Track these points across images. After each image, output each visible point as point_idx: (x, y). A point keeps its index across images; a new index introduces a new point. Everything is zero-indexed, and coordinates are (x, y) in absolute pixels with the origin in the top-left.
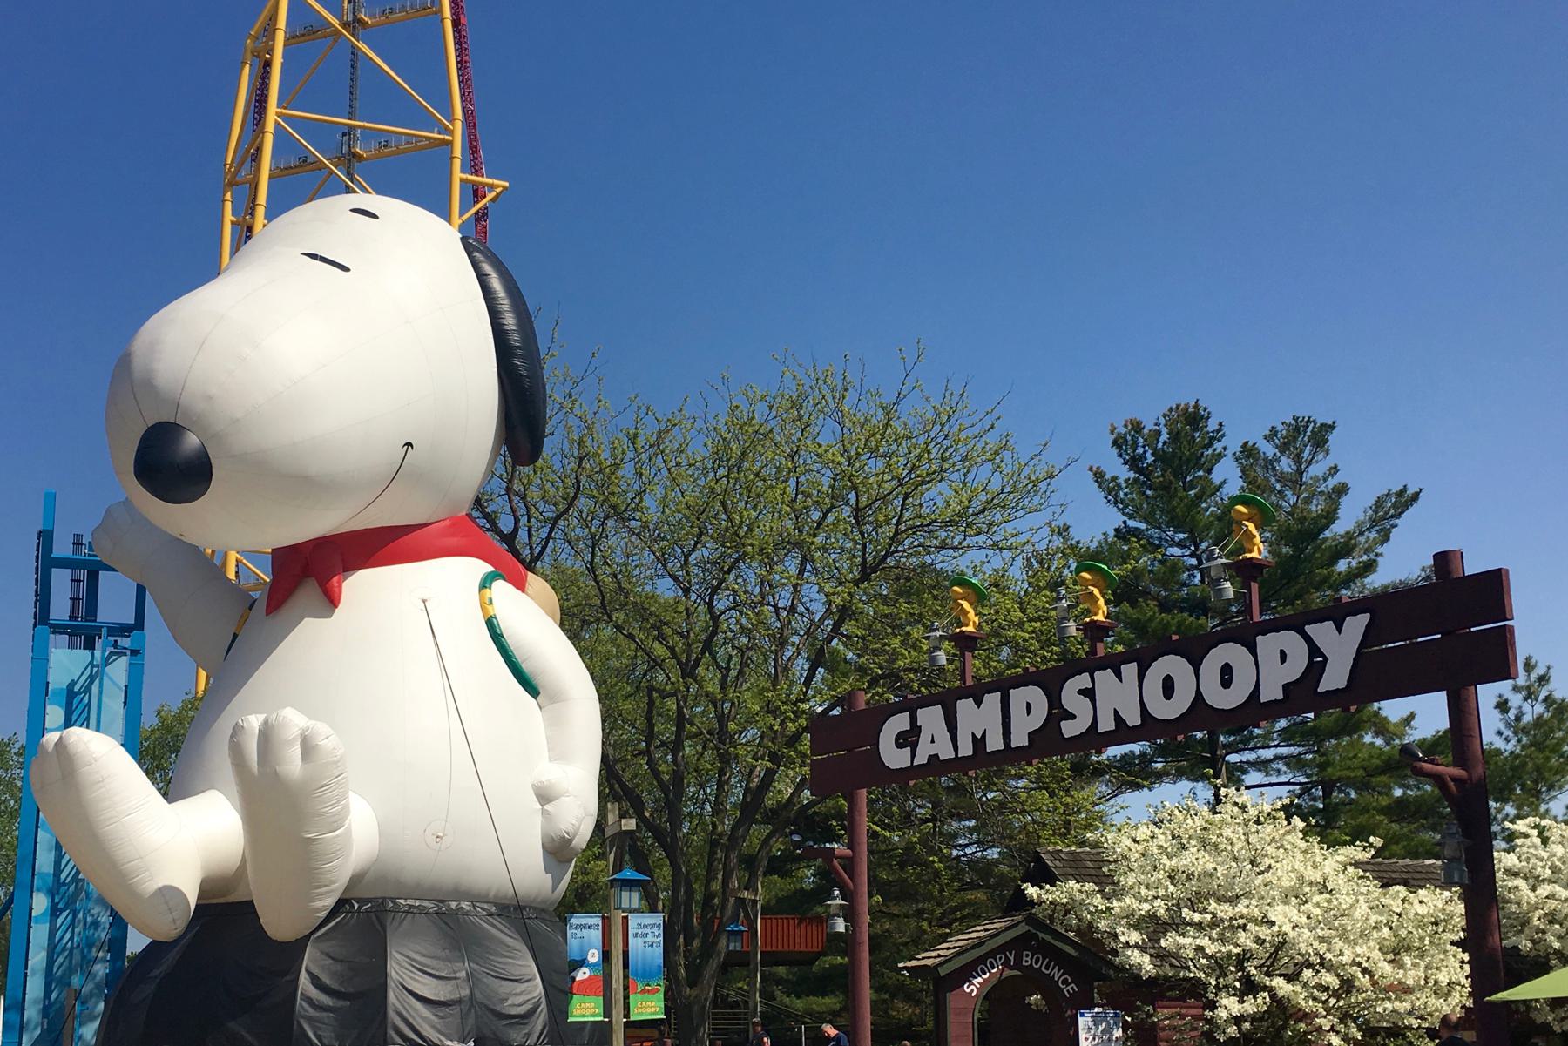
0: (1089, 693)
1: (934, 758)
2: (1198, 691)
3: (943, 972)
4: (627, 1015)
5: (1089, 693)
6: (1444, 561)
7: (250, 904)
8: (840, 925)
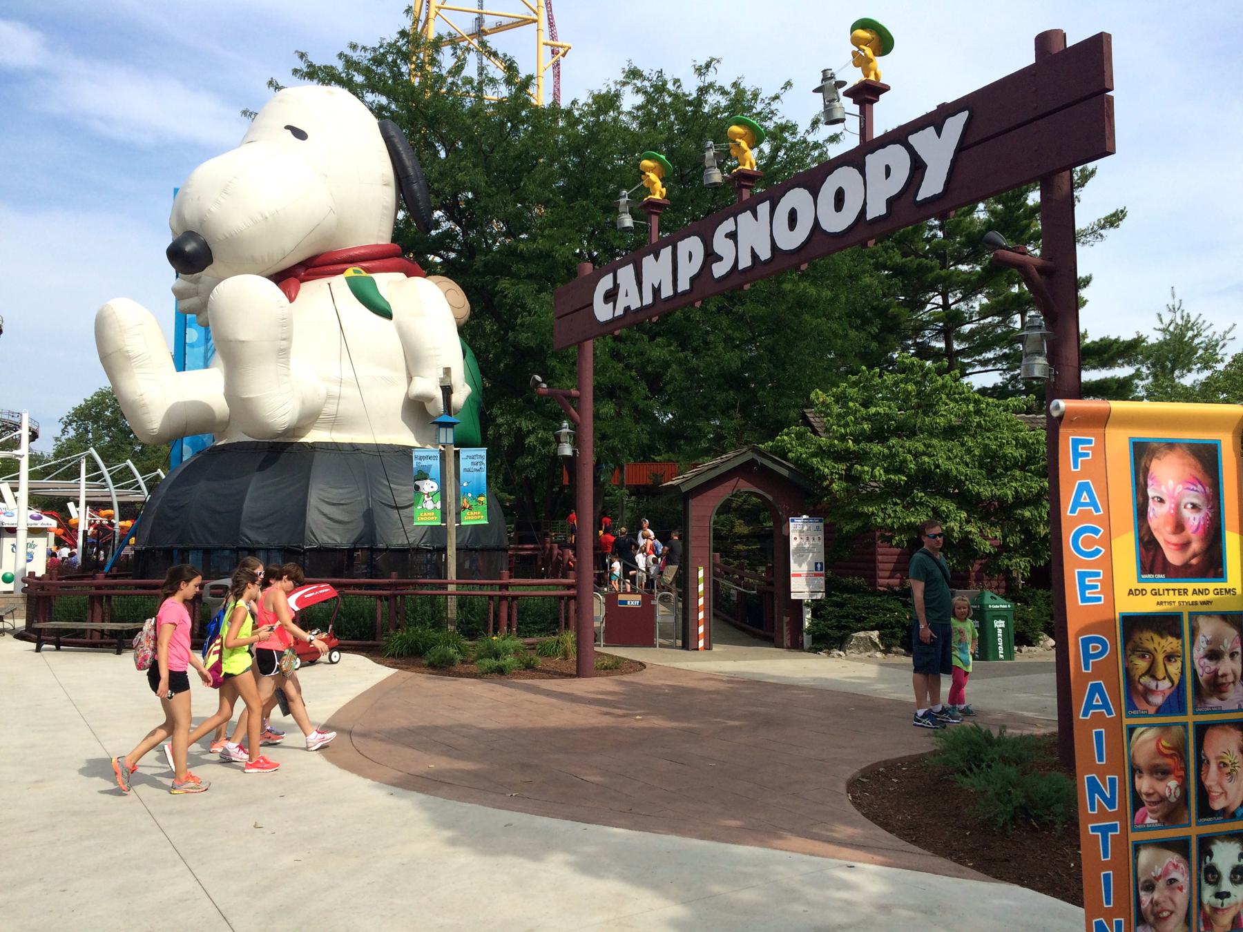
0: (733, 236)
1: (627, 309)
2: (816, 219)
3: (684, 489)
4: (458, 521)
5: (733, 236)
6: (1045, 42)
7: (915, 671)
8: (567, 450)
